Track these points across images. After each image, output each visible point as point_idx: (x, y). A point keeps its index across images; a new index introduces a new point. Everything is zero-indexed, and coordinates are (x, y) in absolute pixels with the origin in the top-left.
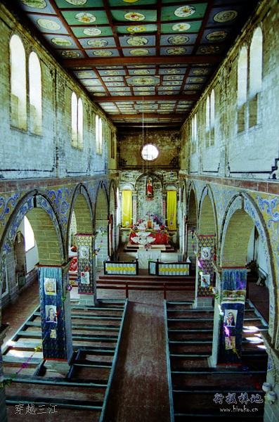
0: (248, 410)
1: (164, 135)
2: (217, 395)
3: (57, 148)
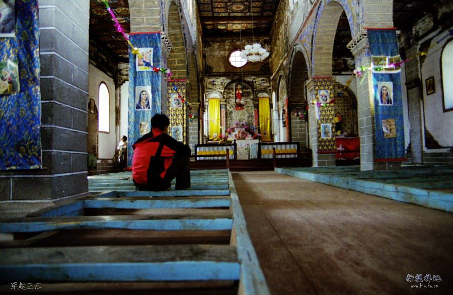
0: (431, 287)
2: (409, 276)
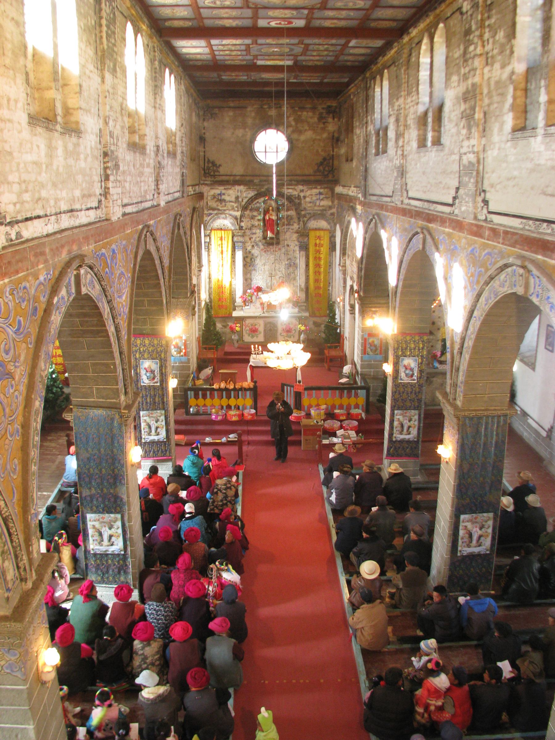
1: (302, 108)
3: (106, 154)
